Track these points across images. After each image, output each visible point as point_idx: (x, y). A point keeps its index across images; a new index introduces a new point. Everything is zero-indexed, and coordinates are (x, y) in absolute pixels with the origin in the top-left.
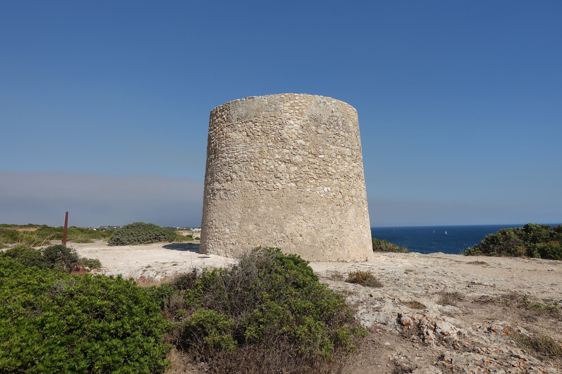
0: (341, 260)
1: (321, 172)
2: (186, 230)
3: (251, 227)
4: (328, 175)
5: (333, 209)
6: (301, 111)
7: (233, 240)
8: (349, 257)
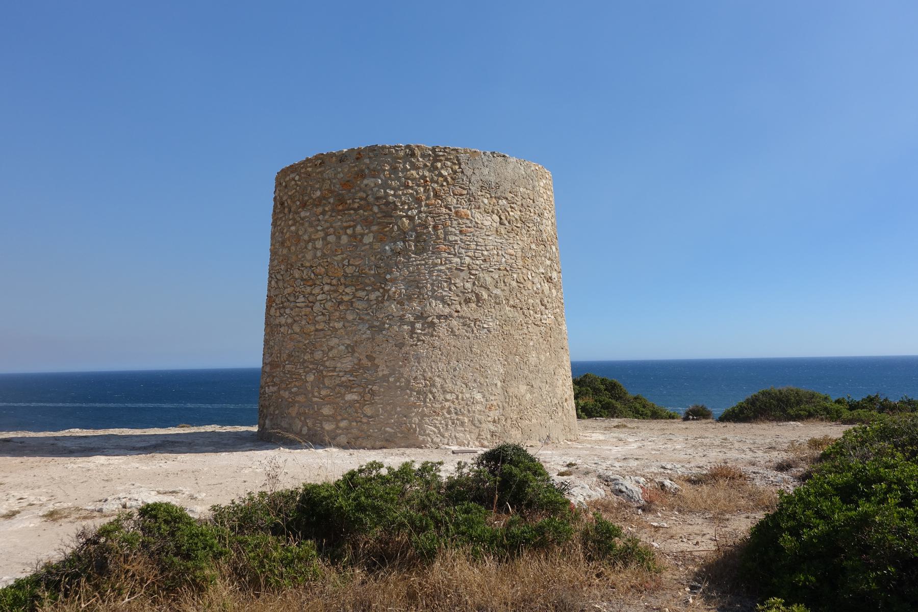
3: (523, 388)
7: (494, 414)
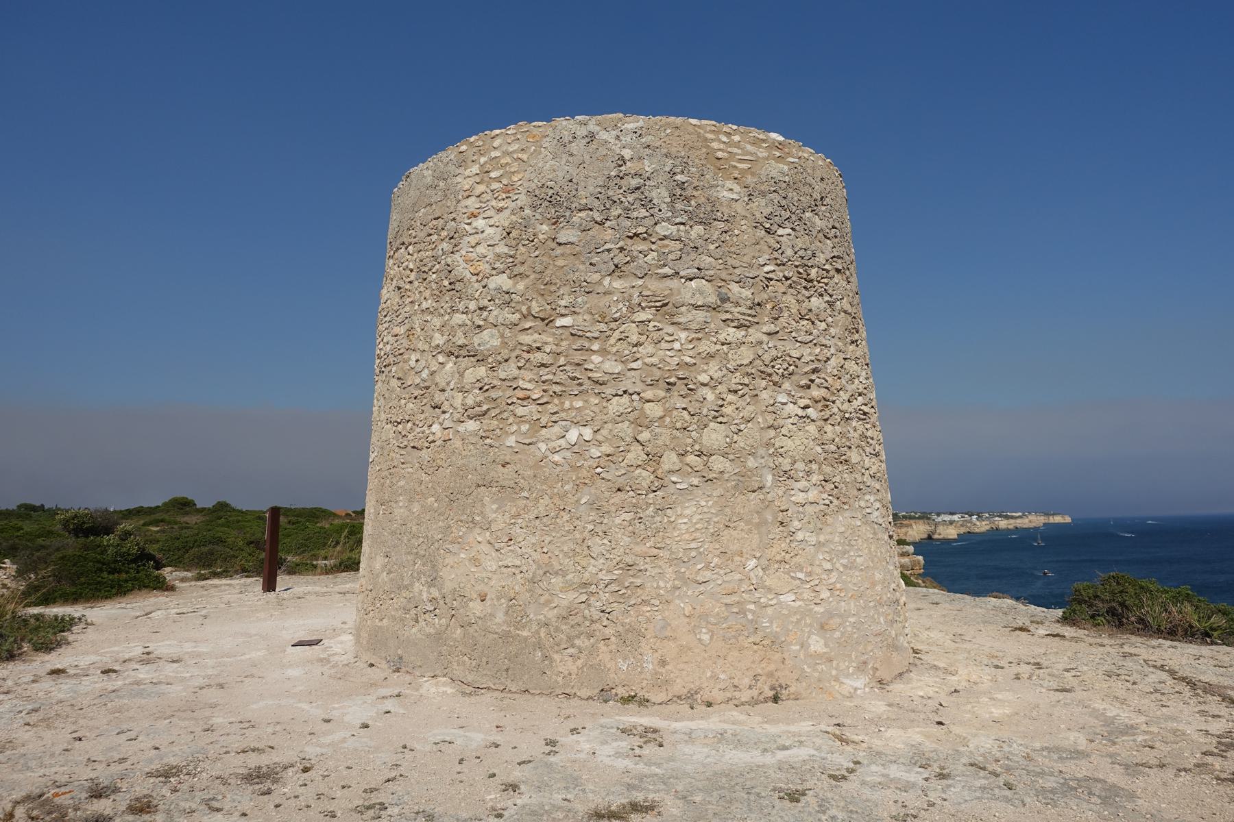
0: (622, 692)
1: (561, 377)
2: (919, 518)
4: (588, 385)
5: (593, 505)
6: (505, 181)
8: (662, 683)
